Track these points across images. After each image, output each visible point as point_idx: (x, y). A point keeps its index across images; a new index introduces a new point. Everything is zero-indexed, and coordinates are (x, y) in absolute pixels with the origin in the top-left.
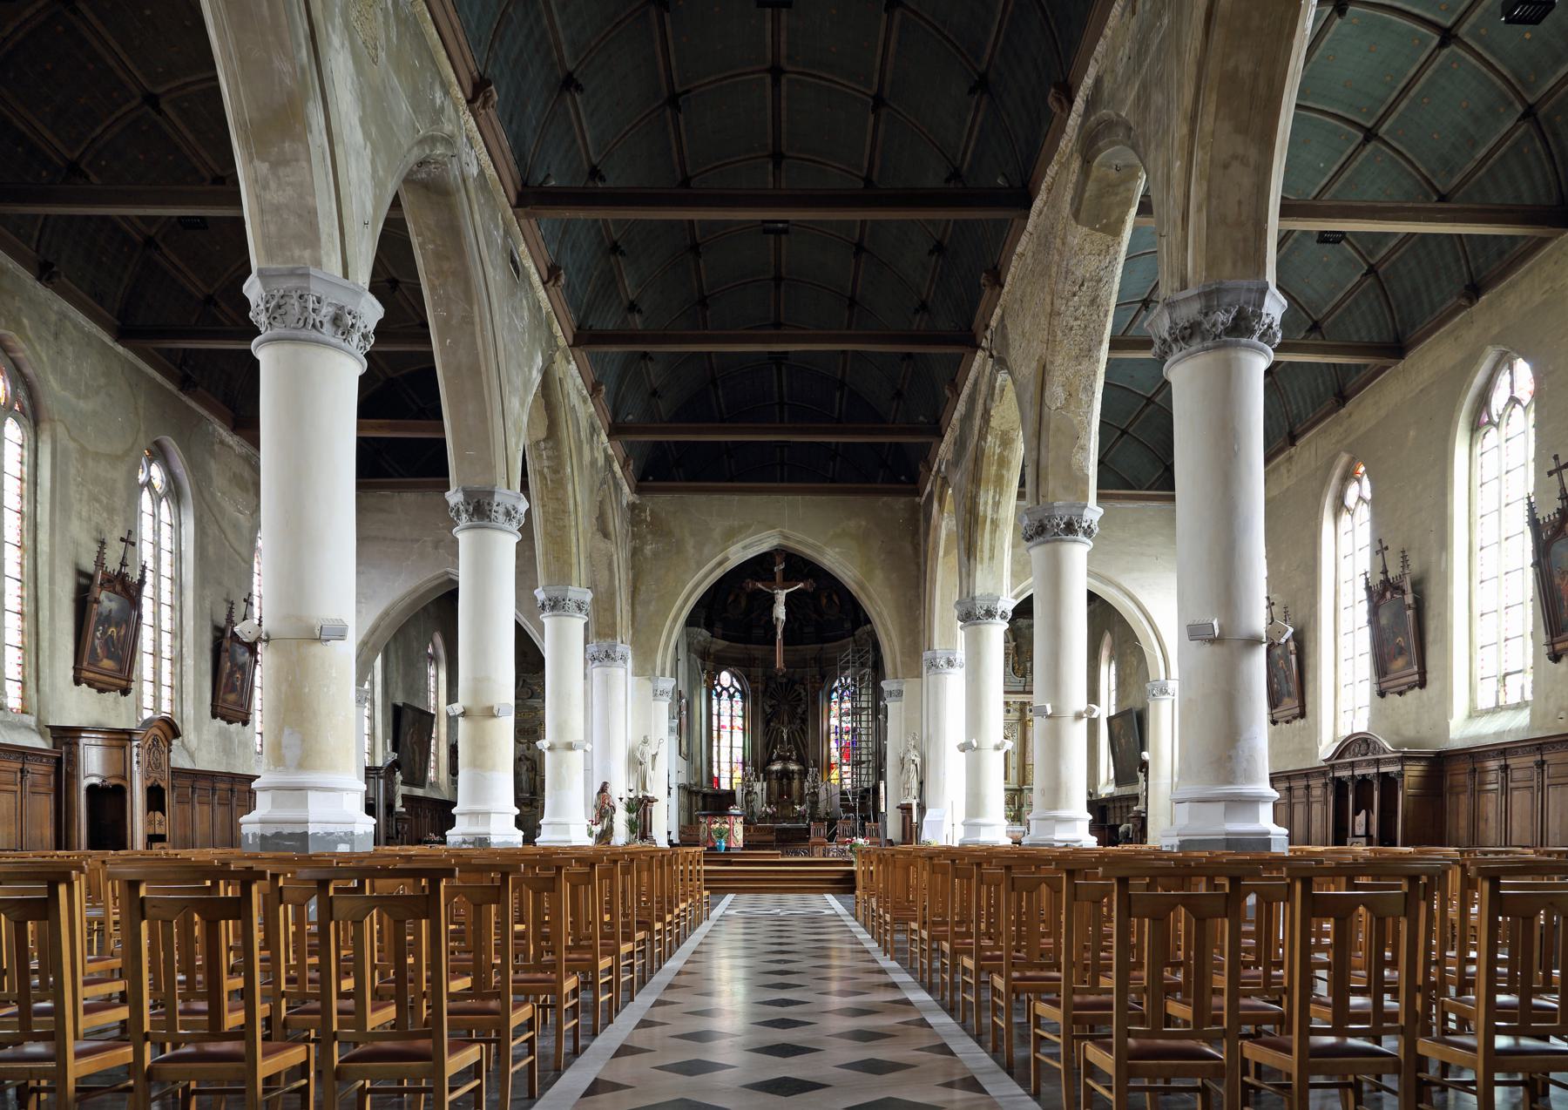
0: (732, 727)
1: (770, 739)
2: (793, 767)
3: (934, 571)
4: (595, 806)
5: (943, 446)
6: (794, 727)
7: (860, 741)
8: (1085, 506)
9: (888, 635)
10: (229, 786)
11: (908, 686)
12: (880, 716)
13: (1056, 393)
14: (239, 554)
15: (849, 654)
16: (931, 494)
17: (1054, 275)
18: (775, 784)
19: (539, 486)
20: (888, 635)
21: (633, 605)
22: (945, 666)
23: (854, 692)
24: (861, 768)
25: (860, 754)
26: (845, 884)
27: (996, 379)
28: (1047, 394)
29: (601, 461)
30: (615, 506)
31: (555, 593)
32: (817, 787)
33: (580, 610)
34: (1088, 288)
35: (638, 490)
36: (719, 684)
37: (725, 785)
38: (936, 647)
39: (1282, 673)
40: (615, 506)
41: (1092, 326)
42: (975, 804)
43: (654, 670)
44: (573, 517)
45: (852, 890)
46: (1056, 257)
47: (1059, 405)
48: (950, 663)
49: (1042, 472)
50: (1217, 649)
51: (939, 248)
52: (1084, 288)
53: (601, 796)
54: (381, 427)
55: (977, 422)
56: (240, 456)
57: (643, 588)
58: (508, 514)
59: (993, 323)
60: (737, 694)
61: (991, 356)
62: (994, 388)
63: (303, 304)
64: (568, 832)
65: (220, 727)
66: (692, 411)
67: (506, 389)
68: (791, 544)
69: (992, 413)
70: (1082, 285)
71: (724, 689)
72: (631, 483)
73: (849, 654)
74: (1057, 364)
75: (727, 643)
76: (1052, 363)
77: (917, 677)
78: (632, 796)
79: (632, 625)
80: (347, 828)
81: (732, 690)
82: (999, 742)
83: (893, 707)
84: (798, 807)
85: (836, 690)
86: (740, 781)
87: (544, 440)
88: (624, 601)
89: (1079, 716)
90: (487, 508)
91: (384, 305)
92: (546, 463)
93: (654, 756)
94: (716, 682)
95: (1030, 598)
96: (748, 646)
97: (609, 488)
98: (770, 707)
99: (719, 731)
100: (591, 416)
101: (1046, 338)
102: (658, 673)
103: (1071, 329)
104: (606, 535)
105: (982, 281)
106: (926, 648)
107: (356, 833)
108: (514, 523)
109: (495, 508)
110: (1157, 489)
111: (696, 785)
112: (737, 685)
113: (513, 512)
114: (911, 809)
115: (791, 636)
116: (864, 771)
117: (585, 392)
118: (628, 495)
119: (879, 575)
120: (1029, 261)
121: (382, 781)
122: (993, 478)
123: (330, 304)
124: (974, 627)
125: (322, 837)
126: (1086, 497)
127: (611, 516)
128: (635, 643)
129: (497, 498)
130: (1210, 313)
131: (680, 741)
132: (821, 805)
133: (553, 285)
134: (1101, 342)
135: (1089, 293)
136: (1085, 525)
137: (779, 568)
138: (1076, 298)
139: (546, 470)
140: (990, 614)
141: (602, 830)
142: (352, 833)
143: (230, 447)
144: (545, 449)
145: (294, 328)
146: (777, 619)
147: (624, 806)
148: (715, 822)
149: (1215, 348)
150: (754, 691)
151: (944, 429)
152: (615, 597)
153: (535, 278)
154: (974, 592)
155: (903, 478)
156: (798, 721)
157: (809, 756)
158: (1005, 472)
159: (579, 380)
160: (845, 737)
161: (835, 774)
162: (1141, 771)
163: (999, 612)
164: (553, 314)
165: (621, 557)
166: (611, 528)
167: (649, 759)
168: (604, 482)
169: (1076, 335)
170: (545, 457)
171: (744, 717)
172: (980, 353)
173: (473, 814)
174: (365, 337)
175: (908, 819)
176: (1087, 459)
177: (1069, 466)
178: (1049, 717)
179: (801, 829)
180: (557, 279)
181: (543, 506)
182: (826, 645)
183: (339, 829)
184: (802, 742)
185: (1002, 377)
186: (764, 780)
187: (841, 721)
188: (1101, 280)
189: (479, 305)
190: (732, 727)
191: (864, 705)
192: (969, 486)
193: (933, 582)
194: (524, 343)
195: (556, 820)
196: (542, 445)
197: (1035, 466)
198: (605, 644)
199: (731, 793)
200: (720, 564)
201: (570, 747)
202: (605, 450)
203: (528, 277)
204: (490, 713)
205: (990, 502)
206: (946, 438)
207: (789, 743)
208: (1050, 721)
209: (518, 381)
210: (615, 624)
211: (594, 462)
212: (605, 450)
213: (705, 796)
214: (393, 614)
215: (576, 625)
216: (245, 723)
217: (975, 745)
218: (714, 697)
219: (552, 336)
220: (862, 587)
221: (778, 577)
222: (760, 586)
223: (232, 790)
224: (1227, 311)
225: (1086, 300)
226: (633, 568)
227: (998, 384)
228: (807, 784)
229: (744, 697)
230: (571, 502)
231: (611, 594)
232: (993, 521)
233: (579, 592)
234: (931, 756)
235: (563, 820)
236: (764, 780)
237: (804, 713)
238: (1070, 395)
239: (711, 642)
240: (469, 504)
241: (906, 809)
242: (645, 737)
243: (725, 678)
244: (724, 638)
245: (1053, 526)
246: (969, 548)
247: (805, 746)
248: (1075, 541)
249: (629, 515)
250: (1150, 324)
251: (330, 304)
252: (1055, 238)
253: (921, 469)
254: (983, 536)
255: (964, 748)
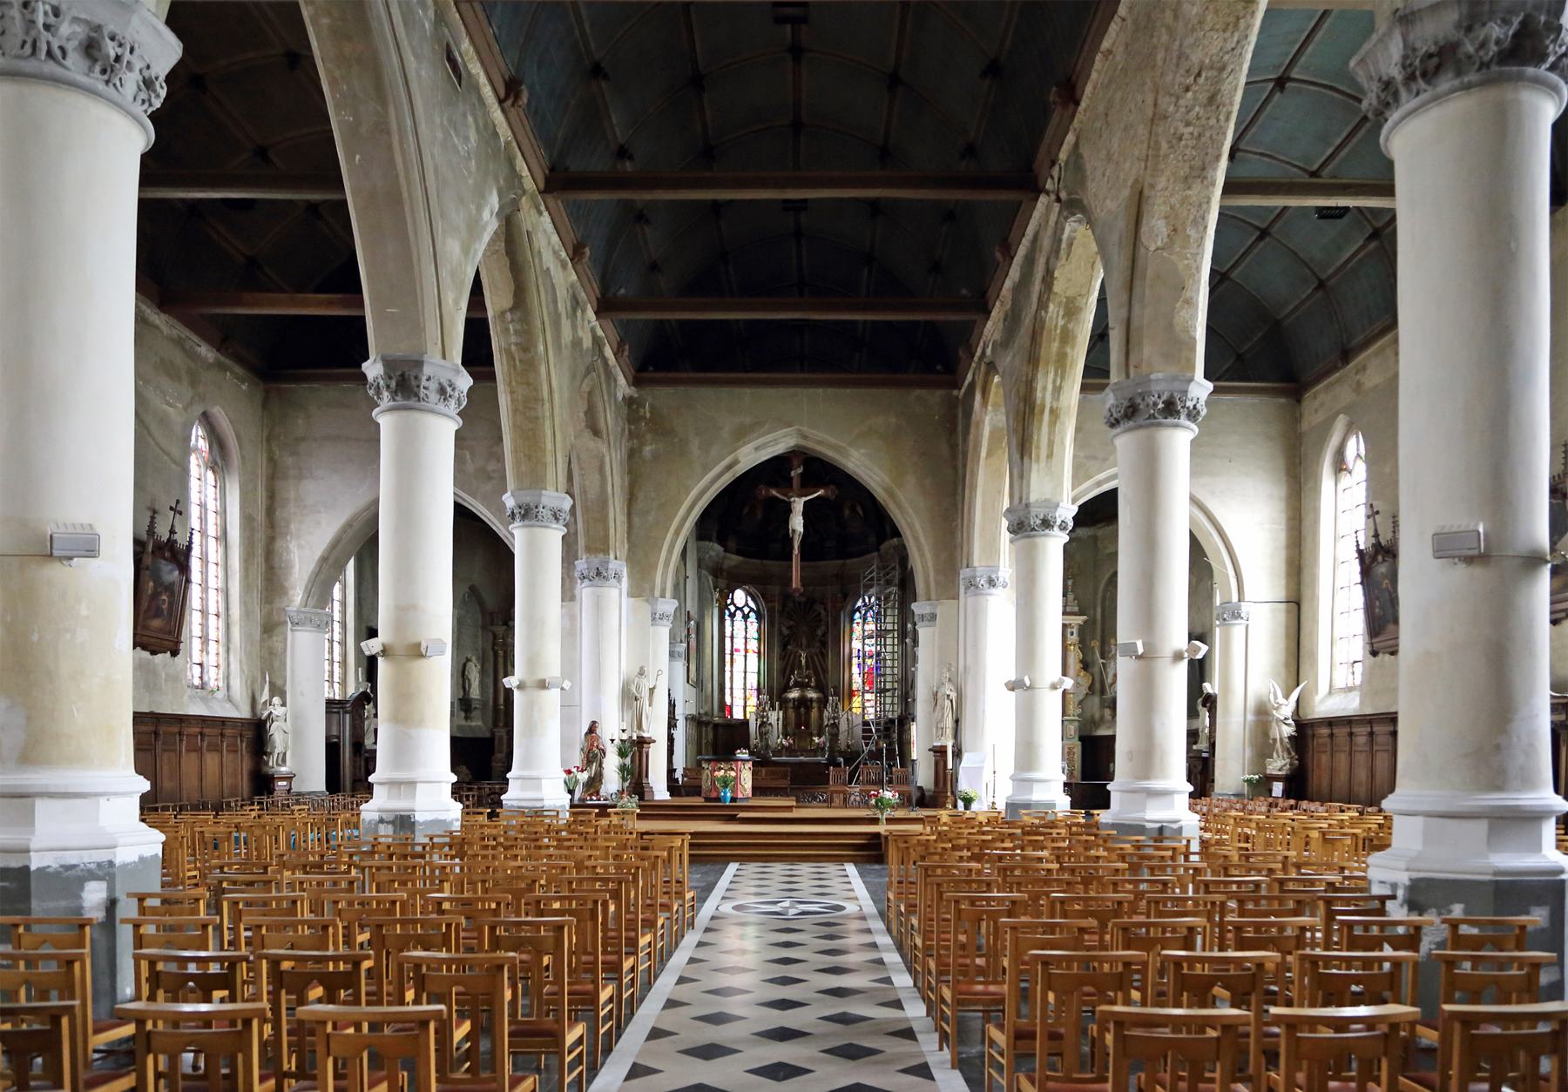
0: (746, 651)
1: (787, 664)
2: (812, 694)
3: (974, 475)
4: (582, 750)
5: (989, 324)
6: (813, 651)
7: (885, 667)
8: (1191, 380)
9: (920, 548)
10: (153, 728)
11: (943, 608)
12: (907, 640)
13: (1156, 227)
14: (168, 454)
15: (873, 571)
16: (972, 386)
17: (1160, 63)
18: (791, 713)
19: (506, 369)
20: (920, 548)
21: (629, 515)
22: (986, 586)
23: (878, 613)
24: (885, 697)
25: (885, 682)
26: (870, 852)
27: (1063, 229)
28: (1144, 229)
29: (587, 342)
30: (606, 398)
31: (527, 499)
32: (837, 718)
33: (557, 519)
34: (1207, 79)
35: (636, 382)
36: (733, 603)
37: (738, 714)
38: (976, 563)
39: (1387, 594)
40: (606, 398)
41: (1208, 134)
42: (1026, 755)
43: (652, 590)
44: (547, 406)
45: (880, 859)
46: (1165, 38)
47: (1159, 244)
48: (991, 583)
49: (1133, 335)
50: (1477, 571)
51: (993, 69)
52: (1201, 80)
53: (589, 736)
54: (330, 304)
55: (1037, 286)
56: (171, 339)
57: (641, 496)
58: (442, 391)
59: (1063, 156)
60: (752, 614)
61: (1058, 200)
62: (1060, 241)
63: (28, 17)
64: (539, 788)
65: (140, 659)
66: (702, 285)
67: (439, 226)
68: (810, 445)
69: (1056, 274)
70: (1199, 75)
71: (737, 608)
72: (628, 373)
73: (873, 571)
74: (1159, 187)
75: (741, 558)
76: (1152, 186)
77: (954, 599)
78: (625, 737)
79: (628, 538)
80: (102, 856)
81: (746, 610)
82: (1056, 680)
83: (924, 632)
84: (816, 739)
85: (858, 610)
86: (754, 709)
87: (511, 310)
88: (618, 510)
89: (1178, 657)
90: (414, 382)
91: (180, 36)
92: (513, 339)
93: (652, 690)
94: (729, 602)
95: (1111, 496)
96: (765, 562)
97: (599, 377)
98: (789, 628)
99: (732, 654)
100: (572, 286)
101: (1144, 152)
102: (657, 593)
103: (1180, 139)
104: (596, 432)
105: (1051, 99)
106: (965, 565)
107: (118, 861)
108: (453, 403)
109: (424, 383)
110: (1226, 380)
111: (706, 714)
112: (752, 604)
113: (449, 389)
114: (946, 752)
115: (810, 549)
116: (889, 700)
117: (563, 254)
118: (623, 387)
119: (911, 480)
120: (1118, 58)
121: (348, 716)
122: (1053, 357)
123: (76, 20)
124: (1027, 540)
125: (57, 874)
126: (1192, 368)
127: (601, 409)
128: (632, 560)
129: (427, 370)
130: (1477, 26)
131: (688, 667)
132: (842, 737)
133: (513, 105)
134: (1218, 158)
135: (1206, 88)
136: (1190, 404)
137: (796, 472)
138: (1190, 95)
139: (513, 348)
140: (1047, 524)
141: (589, 777)
142: (111, 863)
143: (157, 327)
144: (512, 321)
145: (18, 57)
146: (794, 531)
147: (615, 750)
148: (720, 769)
149: (1483, 84)
150: (771, 611)
151: (990, 304)
152: (607, 506)
153: (487, 91)
154: (1028, 498)
155: (939, 367)
156: (818, 644)
157: (833, 688)
158: (1068, 350)
159: (555, 238)
160: (869, 662)
161: (857, 702)
162: (1204, 705)
163: (1059, 522)
164: (515, 144)
165: (614, 459)
166: (602, 424)
167: (645, 694)
168: (589, 370)
169: (1186, 146)
170: (512, 332)
171: (759, 640)
172: (1043, 199)
173: (394, 784)
174: (148, 84)
175: (942, 763)
176: (1194, 316)
177: (1170, 326)
178: (1139, 657)
179: (818, 763)
180: (517, 97)
181: (512, 392)
182: (848, 561)
183: (89, 858)
184: (821, 665)
185: (1074, 228)
186: (780, 709)
187: (864, 644)
188: (1223, 68)
189: (396, 108)
190: (746, 651)
191: (889, 627)
192: (1025, 369)
193: (974, 488)
194: (470, 173)
195: (526, 773)
196: (508, 316)
197: (1124, 327)
198: (596, 560)
199: (744, 723)
200: (729, 467)
201: (543, 685)
202: (593, 330)
203: (476, 89)
204: (417, 652)
205: (1050, 387)
206: (993, 314)
207: (807, 668)
208: (1141, 662)
209: (458, 218)
210: (607, 536)
211: (576, 343)
212: (593, 330)
213: (716, 726)
214: (356, 526)
215: (553, 537)
216: (175, 653)
217: (1028, 683)
218: (727, 617)
219: (514, 175)
220: (891, 494)
221: (796, 483)
222: (774, 492)
223: (156, 734)
224: (1506, 22)
225: (1203, 97)
226: (630, 472)
227: (1065, 237)
228: (826, 713)
229: (759, 618)
230: (545, 387)
231: (603, 502)
232: (1052, 411)
233: (555, 498)
234: (969, 691)
235: (534, 773)
236: (780, 709)
237: (824, 635)
238: (1175, 230)
239: (724, 558)
240: (390, 378)
241: (940, 752)
242: (642, 668)
243: (740, 596)
244: (738, 553)
245: (1148, 405)
246: (1022, 444)
247: (825, 671)
248: (1176, 426)
249: (625, 410)
250: (1362, 60)
251: (76, 20)
252: (1163, 11)
253: (961, 353)
254: (1039, 428)
255: (1012, 686)
